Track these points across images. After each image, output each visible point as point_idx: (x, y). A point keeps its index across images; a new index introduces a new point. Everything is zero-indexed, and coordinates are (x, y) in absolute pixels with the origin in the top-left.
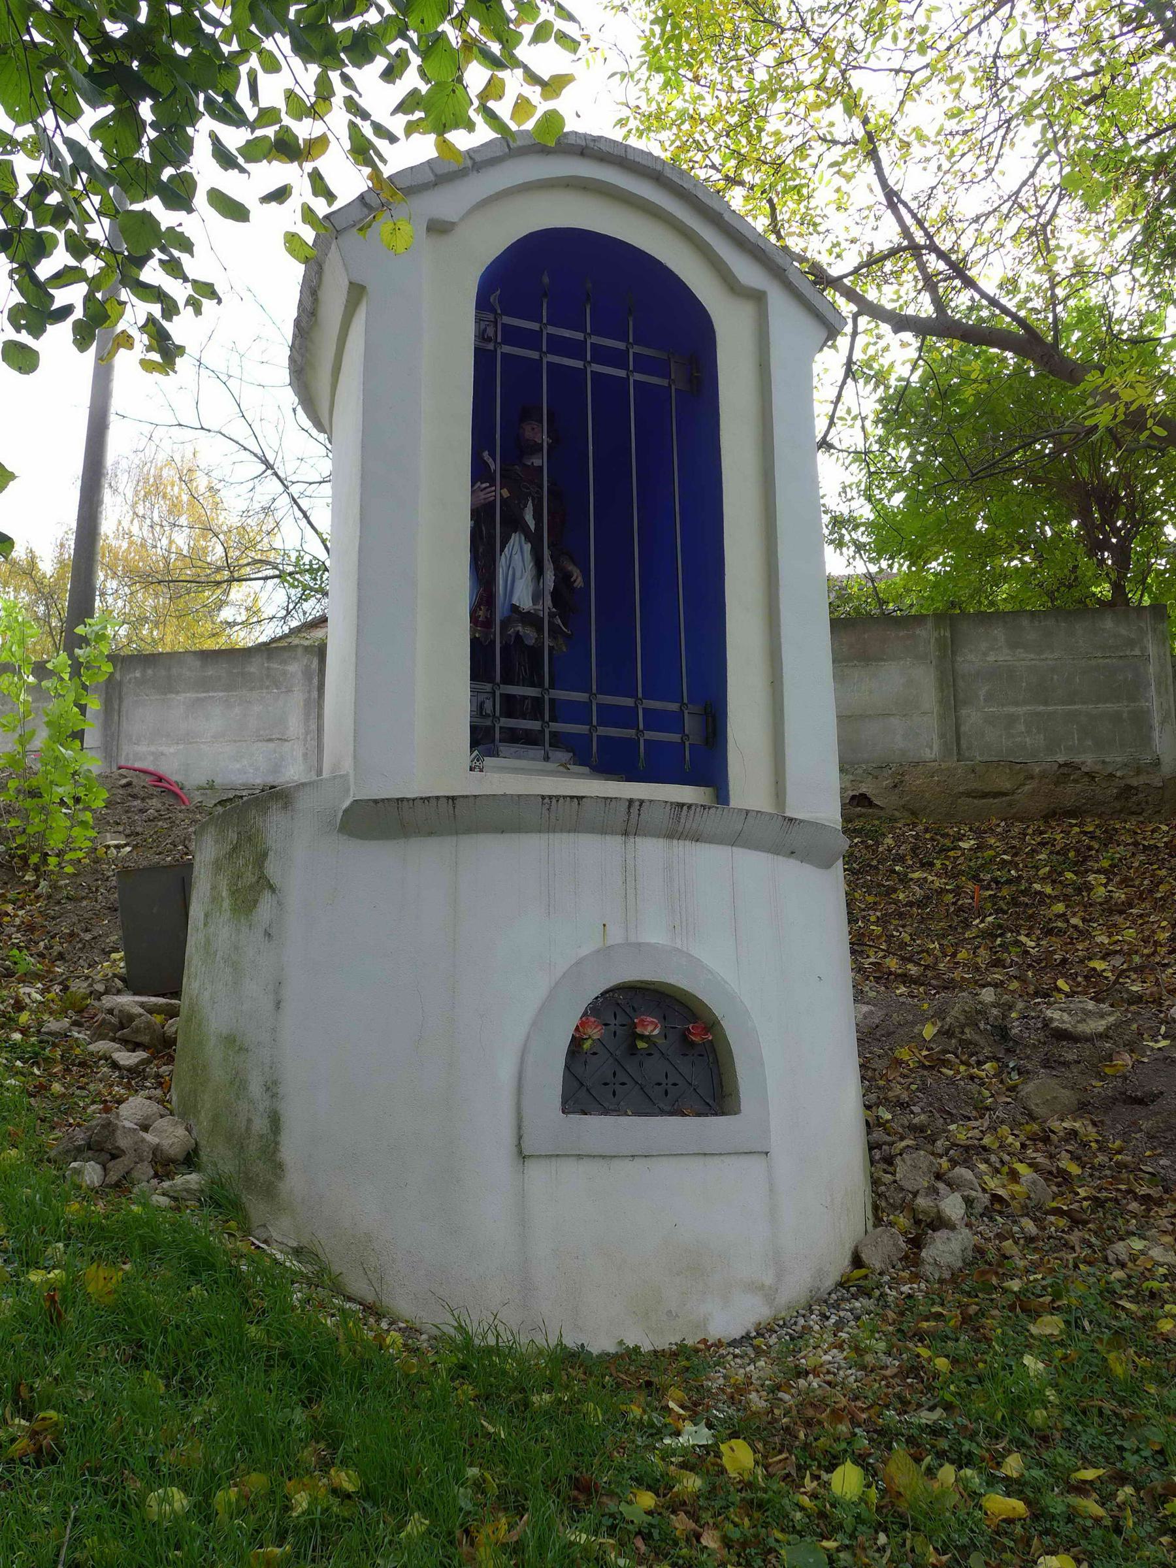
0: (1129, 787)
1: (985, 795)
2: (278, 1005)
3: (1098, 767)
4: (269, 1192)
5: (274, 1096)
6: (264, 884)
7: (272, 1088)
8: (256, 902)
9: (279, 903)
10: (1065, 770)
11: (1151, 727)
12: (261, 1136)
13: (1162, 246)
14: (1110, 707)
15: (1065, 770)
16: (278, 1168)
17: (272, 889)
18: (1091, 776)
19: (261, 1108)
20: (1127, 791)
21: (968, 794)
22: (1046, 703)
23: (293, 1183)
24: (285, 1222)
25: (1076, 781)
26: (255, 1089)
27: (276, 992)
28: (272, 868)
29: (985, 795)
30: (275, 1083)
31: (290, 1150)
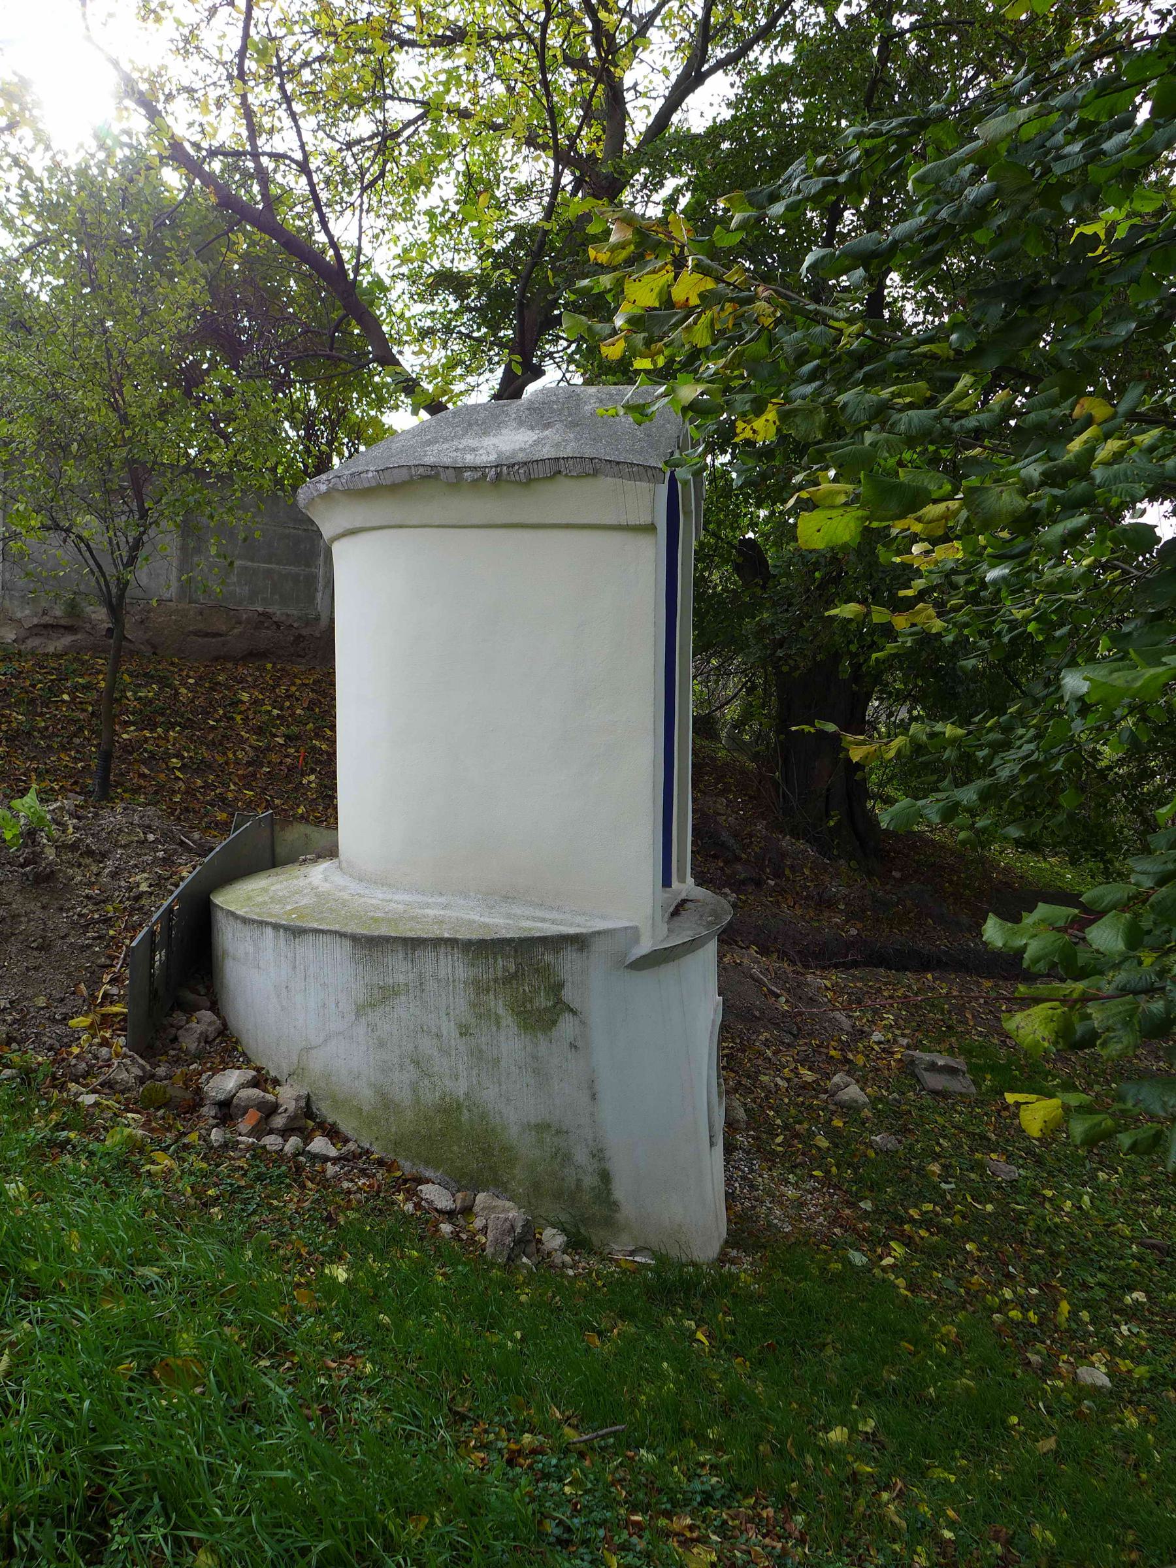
0: (300, 636)
1: (207, 635)
2: (594, 1097)
3: (283, 618)
4: (609, 1223)
5: (601, 1160)
6: (561, 1007)
7: (598, 1154)
8: (554, 1022)
9: (582, 1023)
10: (262, 618)
11: (316, 590)
12: (593, 1189)
13: (726, 458)
14: (293, 569)
15: (262, 618)
16: (614, 1206)
17: (573, 1012)
18: (278, 625)
19: (590, 1169)
20: (299, 638)
21: (196, 633)
22: (252, 560)
23: (628, 1210)
24: (625, 1237)
25: (268, 628)
26: (581, 1156)
27: (591, 1088)
28: (568, 994)
29: (207, 635)
30: (601, 1150)
31: (620, 1192)
